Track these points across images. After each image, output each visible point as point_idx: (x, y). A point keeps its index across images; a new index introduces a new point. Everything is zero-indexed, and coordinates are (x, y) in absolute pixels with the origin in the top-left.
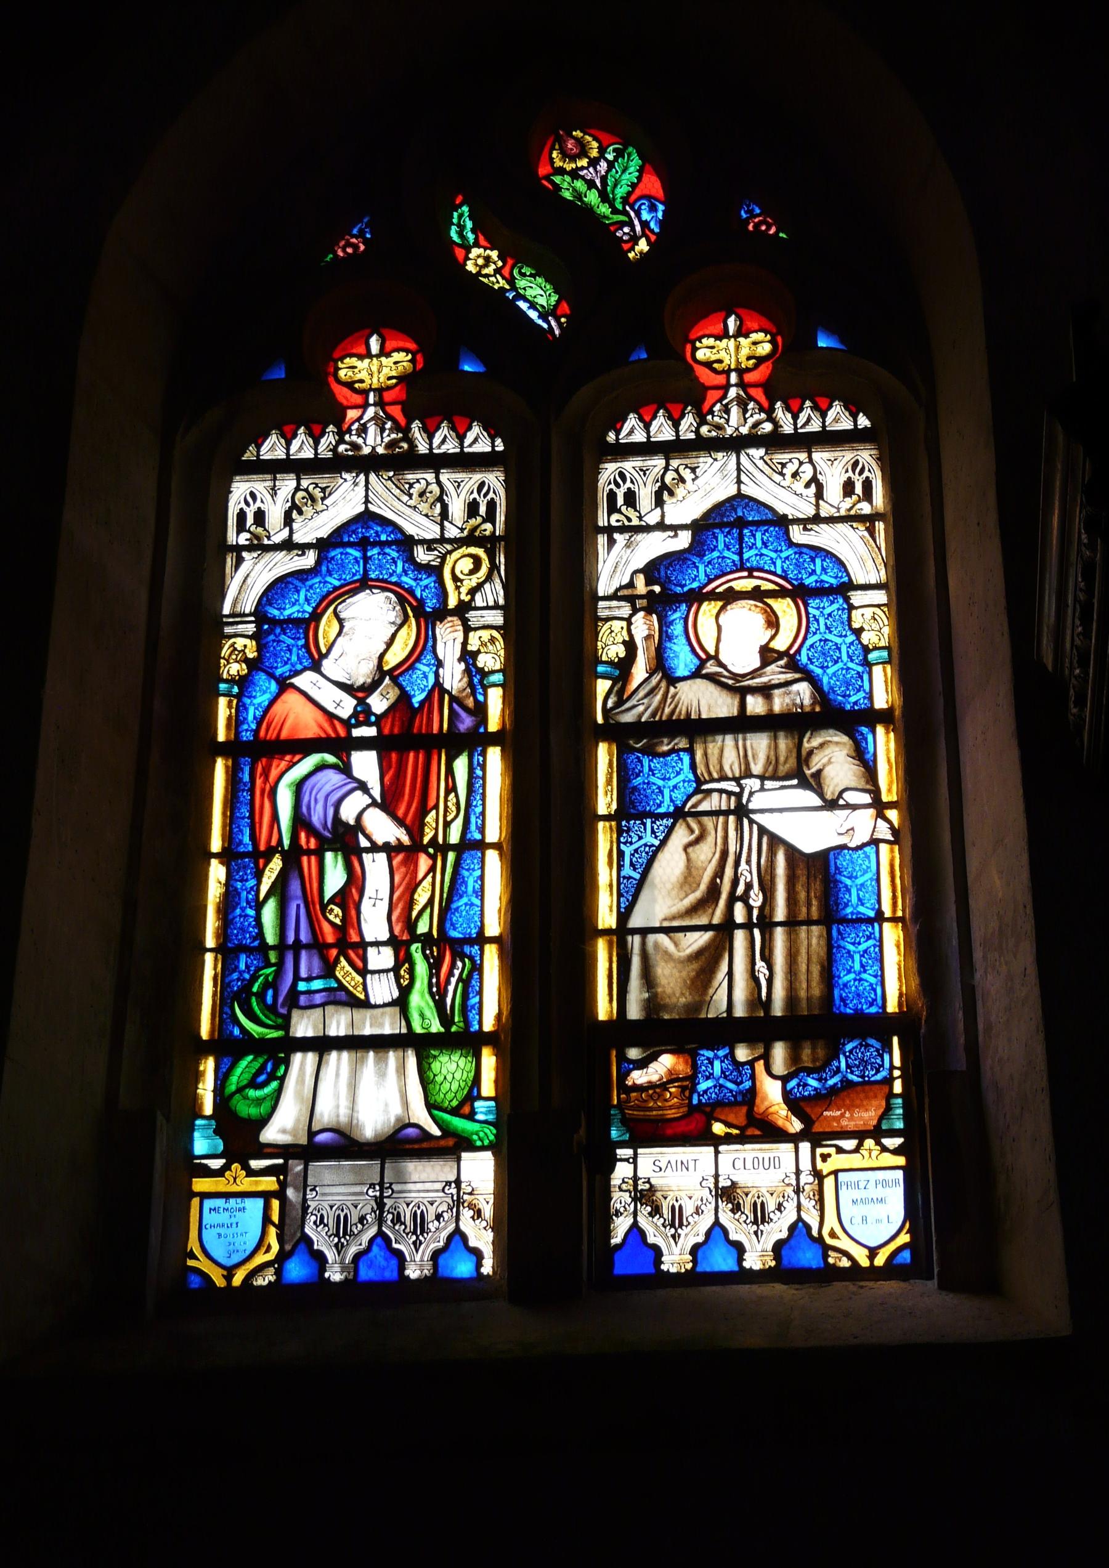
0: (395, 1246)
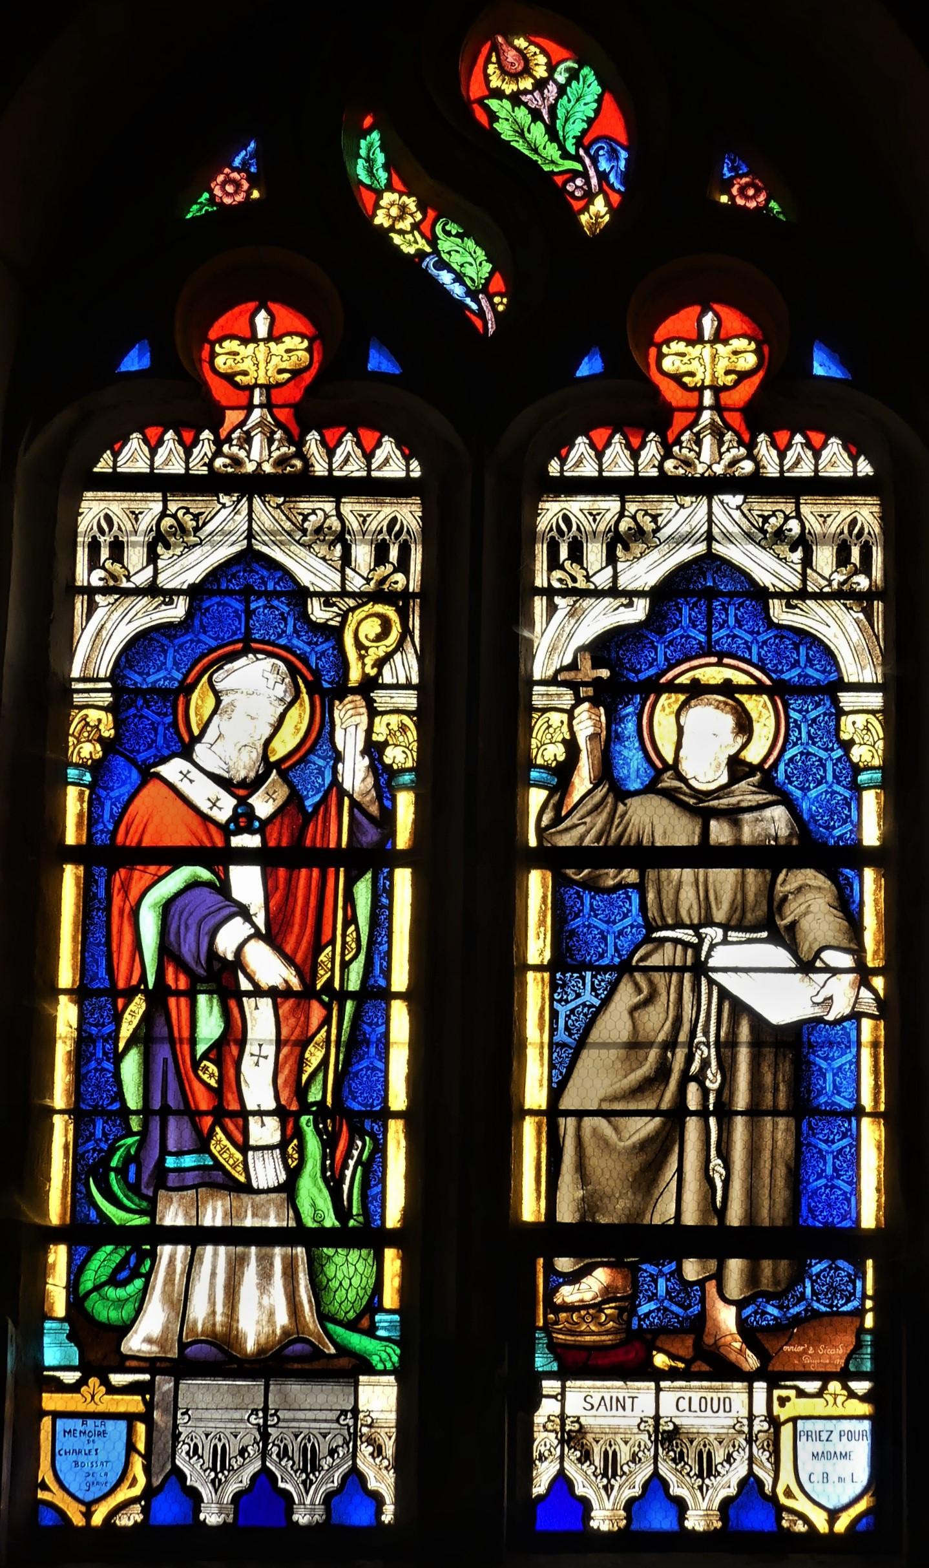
0: (281, 1485)
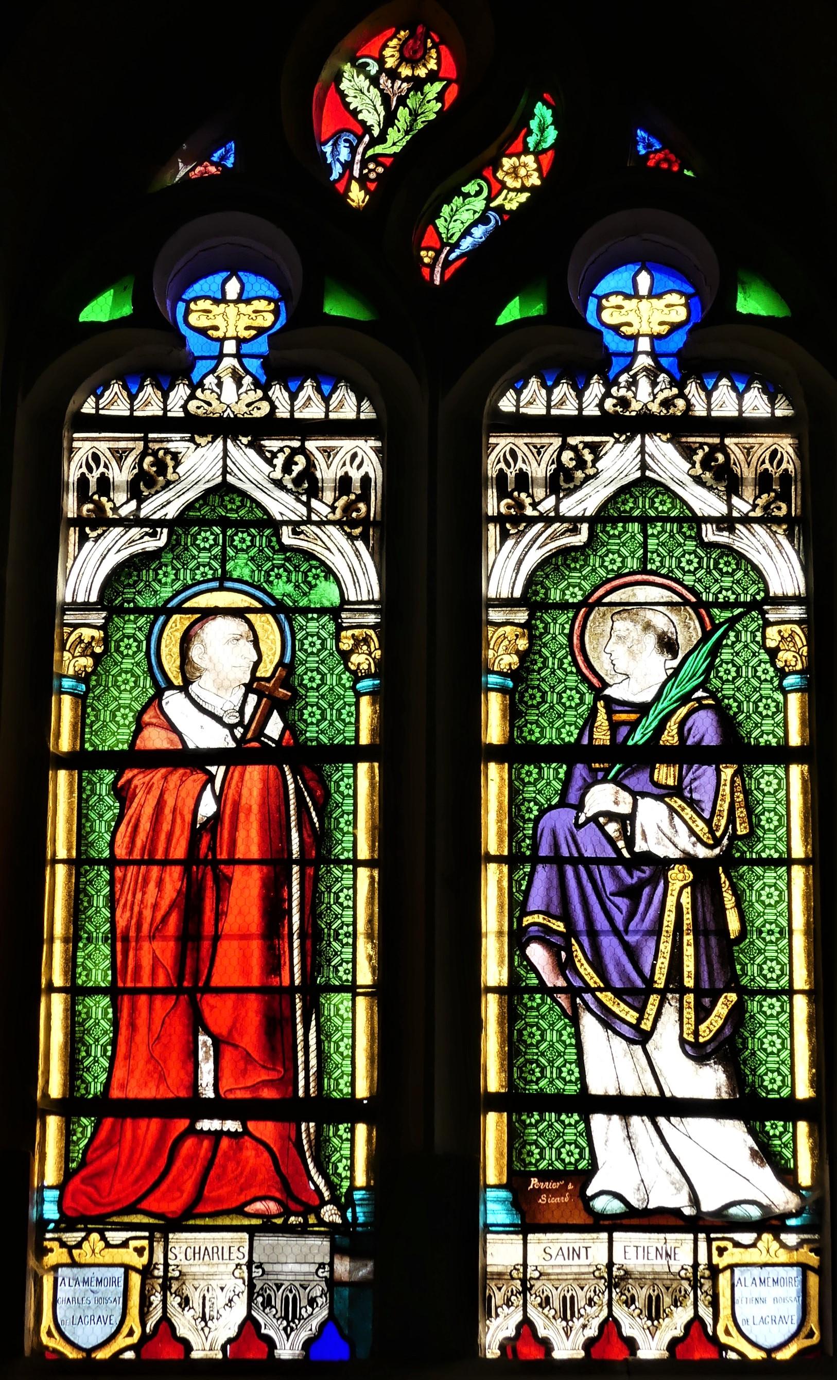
0: (263, 1331)
